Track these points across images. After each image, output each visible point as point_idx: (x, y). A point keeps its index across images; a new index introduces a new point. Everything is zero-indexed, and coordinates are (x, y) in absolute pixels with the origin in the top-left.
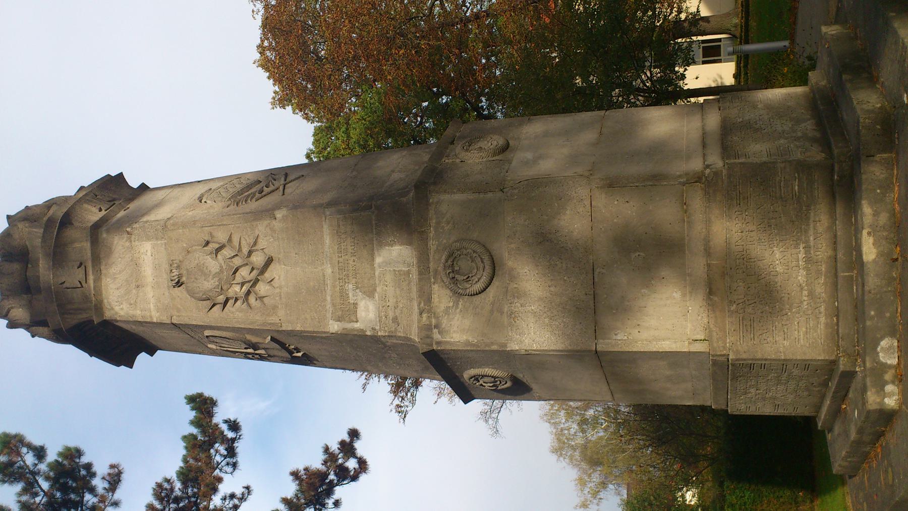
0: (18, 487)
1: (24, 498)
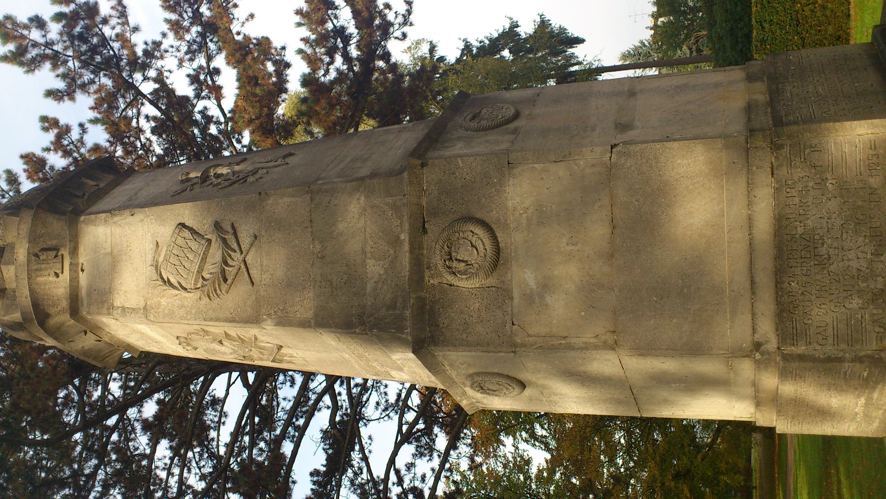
0: (48, 65)
1: (61, 70)
